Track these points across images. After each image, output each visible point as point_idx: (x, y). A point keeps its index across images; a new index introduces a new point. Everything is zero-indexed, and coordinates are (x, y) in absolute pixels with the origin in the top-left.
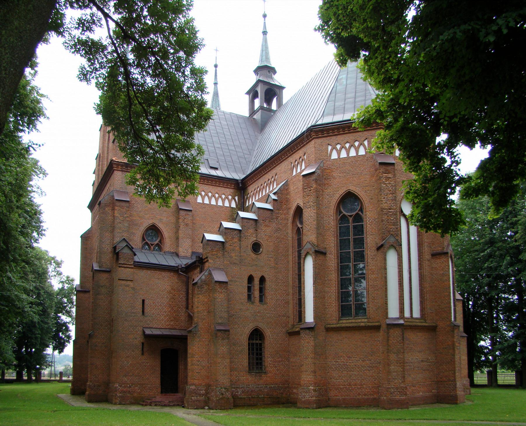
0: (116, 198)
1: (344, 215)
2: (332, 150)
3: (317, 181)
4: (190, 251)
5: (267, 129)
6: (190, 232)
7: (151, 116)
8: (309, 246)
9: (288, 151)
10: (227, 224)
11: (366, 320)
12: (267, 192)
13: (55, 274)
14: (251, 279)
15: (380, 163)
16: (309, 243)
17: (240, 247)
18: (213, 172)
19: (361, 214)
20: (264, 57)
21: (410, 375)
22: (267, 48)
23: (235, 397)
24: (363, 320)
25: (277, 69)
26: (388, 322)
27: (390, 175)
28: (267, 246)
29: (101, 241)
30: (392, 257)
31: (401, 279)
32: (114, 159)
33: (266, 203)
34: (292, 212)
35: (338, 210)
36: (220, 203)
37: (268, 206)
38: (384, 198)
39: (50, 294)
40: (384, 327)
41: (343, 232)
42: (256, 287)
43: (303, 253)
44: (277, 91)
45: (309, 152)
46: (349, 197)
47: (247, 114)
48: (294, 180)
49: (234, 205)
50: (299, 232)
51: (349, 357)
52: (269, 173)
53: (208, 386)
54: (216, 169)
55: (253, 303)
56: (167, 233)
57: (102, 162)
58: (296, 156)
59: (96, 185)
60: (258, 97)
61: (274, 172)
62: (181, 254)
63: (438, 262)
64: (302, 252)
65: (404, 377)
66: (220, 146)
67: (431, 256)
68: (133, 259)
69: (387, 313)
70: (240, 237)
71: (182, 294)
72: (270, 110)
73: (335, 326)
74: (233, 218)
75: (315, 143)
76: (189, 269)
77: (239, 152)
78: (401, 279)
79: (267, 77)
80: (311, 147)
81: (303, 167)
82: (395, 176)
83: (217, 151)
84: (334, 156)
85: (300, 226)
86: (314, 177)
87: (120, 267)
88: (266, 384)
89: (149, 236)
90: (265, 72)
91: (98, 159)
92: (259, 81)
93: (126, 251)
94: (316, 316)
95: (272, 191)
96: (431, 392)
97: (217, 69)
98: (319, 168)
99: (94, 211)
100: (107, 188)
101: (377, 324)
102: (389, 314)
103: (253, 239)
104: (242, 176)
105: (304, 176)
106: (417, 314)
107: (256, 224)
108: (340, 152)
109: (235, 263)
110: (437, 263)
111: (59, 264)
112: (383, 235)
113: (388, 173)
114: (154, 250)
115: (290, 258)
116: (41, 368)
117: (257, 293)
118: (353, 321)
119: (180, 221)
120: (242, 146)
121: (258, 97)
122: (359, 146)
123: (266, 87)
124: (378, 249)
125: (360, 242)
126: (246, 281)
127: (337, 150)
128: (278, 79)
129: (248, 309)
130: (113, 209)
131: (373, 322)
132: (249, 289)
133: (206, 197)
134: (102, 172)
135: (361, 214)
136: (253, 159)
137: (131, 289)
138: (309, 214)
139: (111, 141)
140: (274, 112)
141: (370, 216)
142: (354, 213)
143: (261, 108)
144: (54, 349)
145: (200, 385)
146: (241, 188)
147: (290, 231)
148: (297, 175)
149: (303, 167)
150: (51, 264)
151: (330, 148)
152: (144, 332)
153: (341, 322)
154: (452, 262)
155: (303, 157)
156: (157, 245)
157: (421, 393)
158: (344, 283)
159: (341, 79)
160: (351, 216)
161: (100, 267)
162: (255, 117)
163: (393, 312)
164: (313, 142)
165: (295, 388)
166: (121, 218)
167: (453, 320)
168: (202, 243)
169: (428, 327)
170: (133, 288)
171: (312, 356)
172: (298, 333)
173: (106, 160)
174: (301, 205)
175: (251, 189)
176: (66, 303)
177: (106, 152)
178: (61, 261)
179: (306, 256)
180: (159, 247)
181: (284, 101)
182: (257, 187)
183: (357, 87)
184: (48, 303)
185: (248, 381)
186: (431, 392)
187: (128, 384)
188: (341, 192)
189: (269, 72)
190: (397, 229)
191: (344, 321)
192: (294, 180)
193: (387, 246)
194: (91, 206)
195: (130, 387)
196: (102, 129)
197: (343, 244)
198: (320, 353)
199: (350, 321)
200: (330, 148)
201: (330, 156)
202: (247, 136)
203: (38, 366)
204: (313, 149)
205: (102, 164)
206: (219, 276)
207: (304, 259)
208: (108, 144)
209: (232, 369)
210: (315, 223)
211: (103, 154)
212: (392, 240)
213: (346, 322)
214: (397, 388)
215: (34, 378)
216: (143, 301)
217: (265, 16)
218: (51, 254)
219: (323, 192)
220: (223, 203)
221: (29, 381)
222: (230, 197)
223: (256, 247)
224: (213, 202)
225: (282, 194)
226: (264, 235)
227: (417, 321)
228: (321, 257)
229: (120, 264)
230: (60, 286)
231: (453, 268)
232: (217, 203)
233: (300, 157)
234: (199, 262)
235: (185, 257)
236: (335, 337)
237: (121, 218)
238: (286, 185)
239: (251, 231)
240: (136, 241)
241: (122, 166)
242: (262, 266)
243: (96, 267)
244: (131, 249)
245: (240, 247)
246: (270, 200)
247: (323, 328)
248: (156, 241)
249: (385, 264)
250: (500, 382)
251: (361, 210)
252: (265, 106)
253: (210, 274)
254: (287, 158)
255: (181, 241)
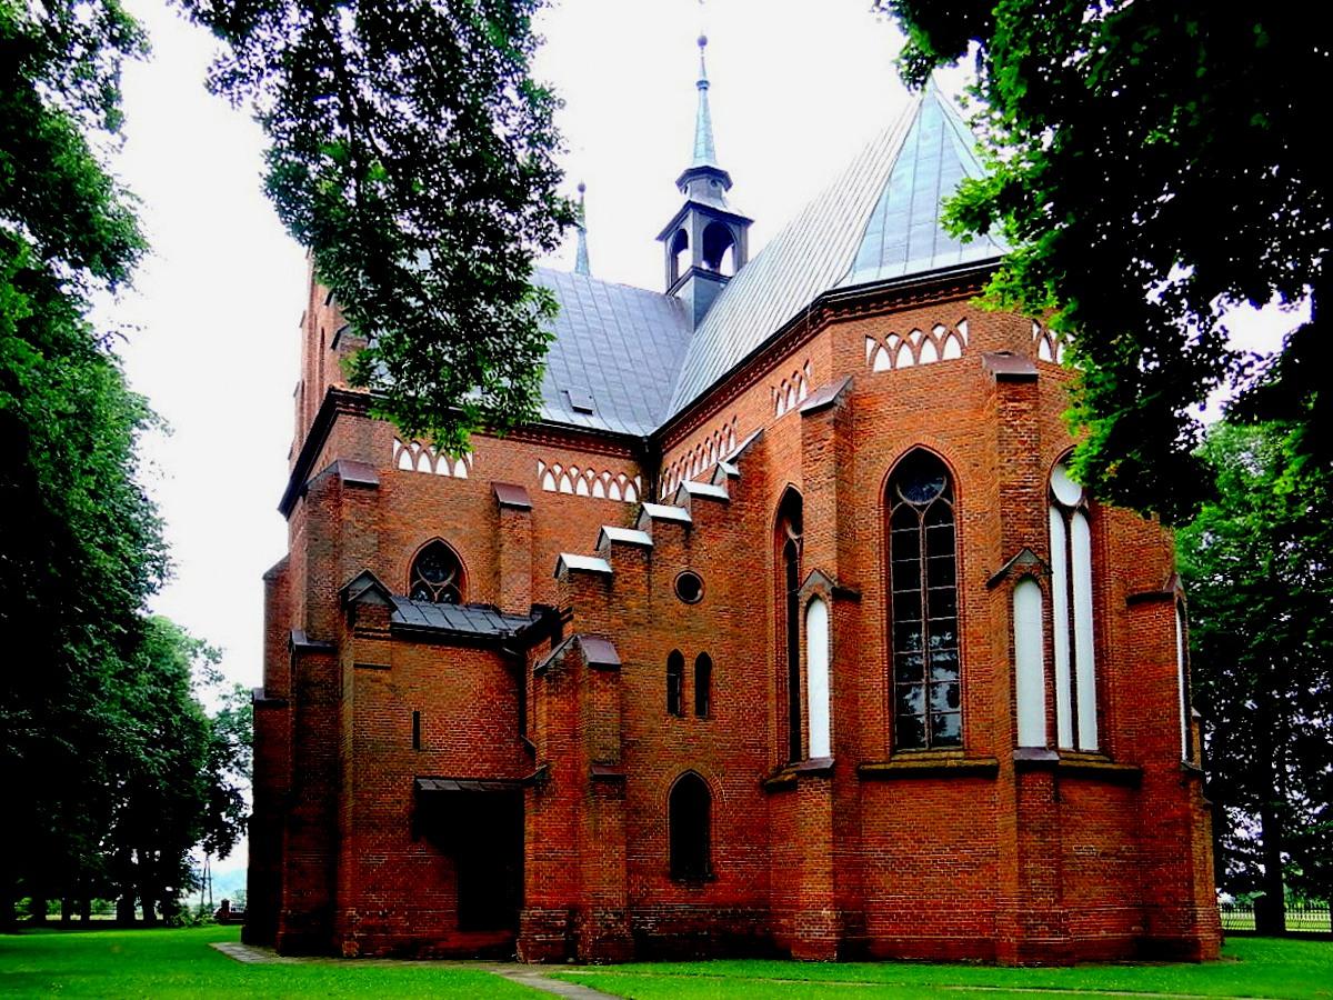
0: (344, 477)
1: (905, 505)
2: (875, 350)
3: (842, 420)
4: (528, 601)
5: (709, 323)
6: (528, 559)
7: (421, 231)
8: (818, 579)
9: (765, 359)
10: (615, 533)
11: (960, 754)
12: (714, 460)
13: (208, 679)
14: (675, 661)
15: (1002, 378)
16: (819, 571)
17: (649, 587)
18: (580, 420)
19: (949, 502)
20: (702, 147)
21: (1073, 887)
22: (707, 122)
23: (640, 935)
24: (953, 754)
25: (732, 177)
26: (1018, 755)
27: (1024, 406)
28: (715, 584)
29: (309, 578)
30: (1027, 602)
31: (1046, 667)
32: (337, 386)
33: (712, 483)
34: (773, 505)
35: (890, 496)
36: (598, 491)
37: (720, 492)
38: (1009, 461)
39: (195, 726)
40: (1007, 769)
41: (900, 545)
42: (690, 683)
43: (804, 595)
44: (735, 229)
45: (817, 357)
46: (920, 469)
47: (661, 286)
48: (779, 428)
49: (631, 496)
50: (792, 554)
51: (919, 841)
52: (717, 416)
53: (574, 910)
54: (589, 412)
55: (682, 715)
56: (471, 562)
57: (309, 399)
58: (785, 370)
59: (297, 455)
60: (686, 247)
61: (728, 412)
62: (507, 608)
63: (1147, 621)
64: (802, 593)
65: (1060, 891)
66: (595, 360)
67: (1126, 597)
68: (390, 618)
69: (1015, 737)
70: (649, 561)
71: (509, 699)
72: (718, 278)
73: (881, 767)
74: (632, 516)
75: (833, 335)
76: (528, 639)
77: (643, 375)
78: (1046, 667)
79: (710, 195)
80: (822, 348)
81: (803, 396)
82: (1036, 407)
83: (588, 372)
84: (882, 362)
85: (793, 536)
86: (830, 416)
87: (357, 636)
88: (713, 907)
89: (430, 568)
90: (703, 182)
91: (299, 395)
92: (690, 205)
93: (372, 599)
94: (839, 742)
95: (725, 458)
96: (1129, 931)
97: (585, 194)
98: (843, 393)
99: (293, 518)
100: (322, 458)
101: (989, 762)
102: (1019, 740)
103: (681, 568)
104: (650, 430)
105: (805, 414)
106: (1089, 742)
107: (687, 534)
108: (897, 353)
109: (636, 623)
110: (1144, 621)
111: (214, 656)
112: (1007, 551)
113: (1019, 401)
114: (440, 600)
115: (771, 612)
116: (176, 894)
117: (690, 694)
118: (929, 755)
119: (503, 531)
120: (650, 362)
121: (686, 247)
122: (945, 338)
123: (708, 220)
124: (992, 584)
125: (944, 571)
126: (664, 665)
127: (888, 350)
128: (732, 202)
129: (668, 731)
130: (338, 505)
131: (980, 759)
132: (672, 683)
133: (598, 483)
134: (309, 424)
135: (949, 502)
136: (677, 392)
137: (386, 689)
138: (819, 509)
139: (328, 344)
140: (726, 280)
141: (975, 506)
142: (932, 501)
143: (697, 271)
144: (208, 849)
145: (556, 906)
146: (645, 457)
147: (770, 551)
148: (787, 416)
149: (803, 396)
150: (196, 656)
151: (541, 467)
152: (417, 786)
153: (897, 757)
154: (1182, 619)
155: (801, 372)
156: (448, 589)
157: (1103, 933)
158: (904, 674)
159: (898, 179)
160: (922, 508)
161: (309, 640)
162: (679, 294)
163: (1031, 734)
164: (828, 331)
165: (784, 915)
166: (360, 526)
167: (1184, 757)
168: (556, 576)
169: (1122, 773)
170: (392, 687)
171: (828, 836)
172: (791, 787)
173: (317, 393)
174: (799, 486)
175: (672, 459)
176: (235, 745)
177: (317, 375)
178: (220, 650)
179: (810, 602)
180: (456, 599)
181: (752, 253)
182: (687, 452)
183: (943, 180)
184: (190, 739)
185: (673, 899)
186: (1129, 931)
187: (380, 908)
188: (900, 449)
189: (714, 182)
190: (1040, 534)
191: (906, 757)
192: (779, 428)
193: (1014, 574)
194: (287, 507)
195: (385, 915)
196: (306, 324)
197: (902, 575)
198: (847, 827)
199: (920, 756)
200: (870, 344)
201: (872, 365)
202: (662, 339)
203: (169, 889)
204: (829, 350)
205: (308, 404)
206: (597, 653)
207: (807, 610)
208: (322, 353)
209: (633, 869)
210: (833, 524)
211: (309, 381)
212: (1028, 561)
213: (909, 759)
214: (1044, 917)
215: (160, 917)
216: (417, 715)
217: (703, 42)
218: (195, 634)
219: (852, 450)
220: (607, 492)
221: (150, 922)
222: (622, 479)
223: (688, 587)
224: (582, 489)
225: (749, 463)
226: (711, 556)
227: (1092, 758)
228: (849, 607)
229: (357, 629)
230: (221, 706)
231: (1183, 631)
232: (591, 492)
233: (796, 372)
234: (548, 624)
235: (515, 616)
236: (884, 793)
237: (360, 526)
238: (760, 440)
239: (676, 548)
240: (398, 578)
241: (355, 401)
242: (703, 630)
243: (299, 640)
244: (385, 595)
245: (649, 587)
246: (721, 476)
247: (852, 772)
248: (445, 579)
249: (1011, 618)
250: (1290, 927)
251: (948, 493)
252: (705, 266)
253: (576, 647)
254: (761, 378)
255: (505, 579)
